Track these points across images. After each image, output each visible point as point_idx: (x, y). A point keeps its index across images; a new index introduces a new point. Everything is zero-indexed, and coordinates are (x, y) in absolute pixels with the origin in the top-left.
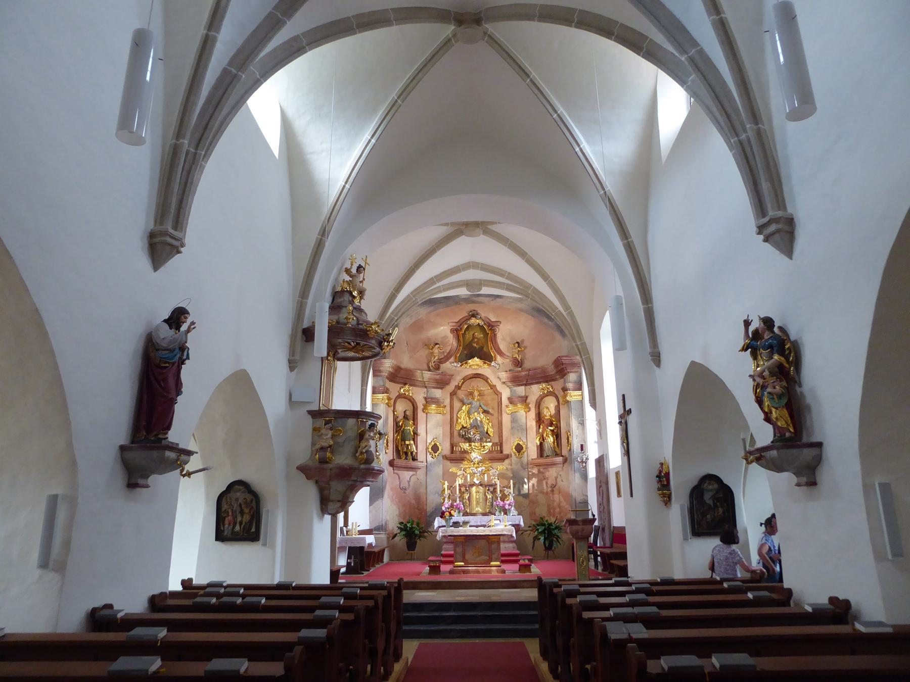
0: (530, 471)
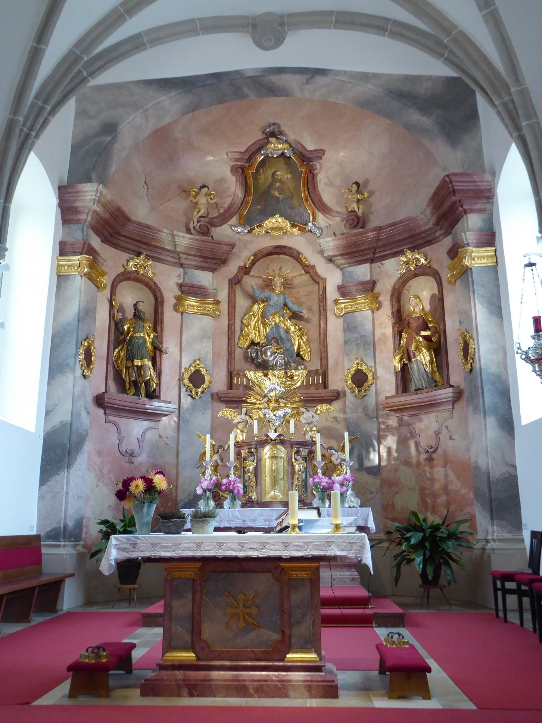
0: (384, 423)
